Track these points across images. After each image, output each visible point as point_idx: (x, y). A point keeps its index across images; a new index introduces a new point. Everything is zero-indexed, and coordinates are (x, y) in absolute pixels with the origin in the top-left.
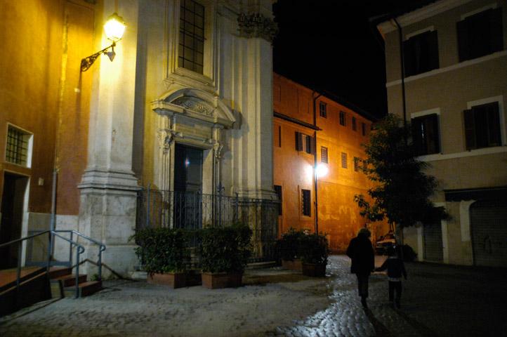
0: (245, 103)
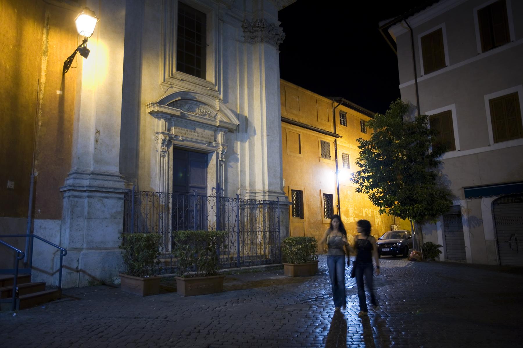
0: (251, 106)
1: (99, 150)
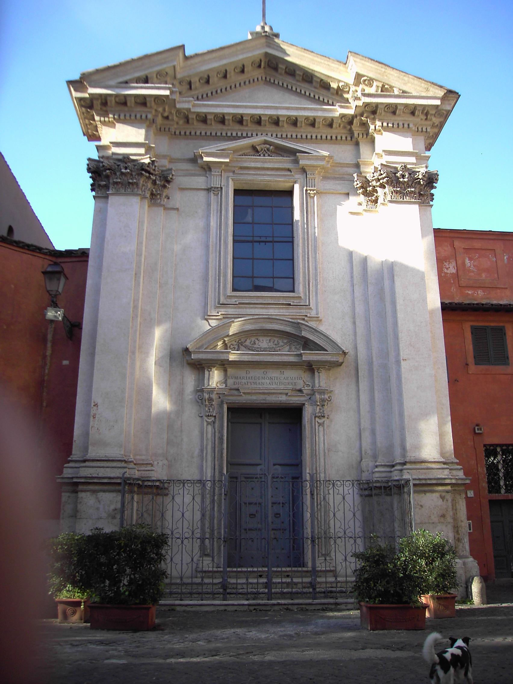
1: (96, 428)
